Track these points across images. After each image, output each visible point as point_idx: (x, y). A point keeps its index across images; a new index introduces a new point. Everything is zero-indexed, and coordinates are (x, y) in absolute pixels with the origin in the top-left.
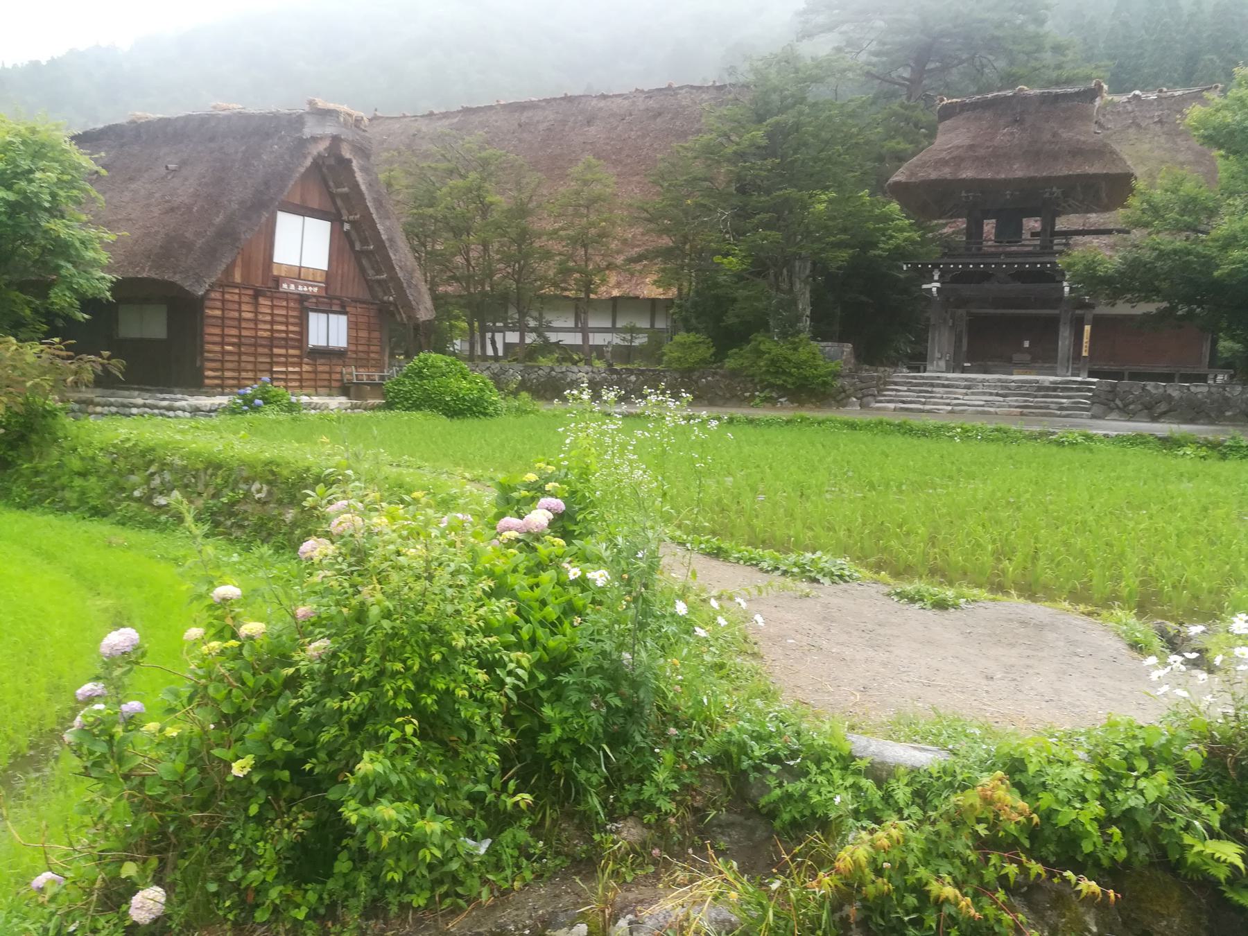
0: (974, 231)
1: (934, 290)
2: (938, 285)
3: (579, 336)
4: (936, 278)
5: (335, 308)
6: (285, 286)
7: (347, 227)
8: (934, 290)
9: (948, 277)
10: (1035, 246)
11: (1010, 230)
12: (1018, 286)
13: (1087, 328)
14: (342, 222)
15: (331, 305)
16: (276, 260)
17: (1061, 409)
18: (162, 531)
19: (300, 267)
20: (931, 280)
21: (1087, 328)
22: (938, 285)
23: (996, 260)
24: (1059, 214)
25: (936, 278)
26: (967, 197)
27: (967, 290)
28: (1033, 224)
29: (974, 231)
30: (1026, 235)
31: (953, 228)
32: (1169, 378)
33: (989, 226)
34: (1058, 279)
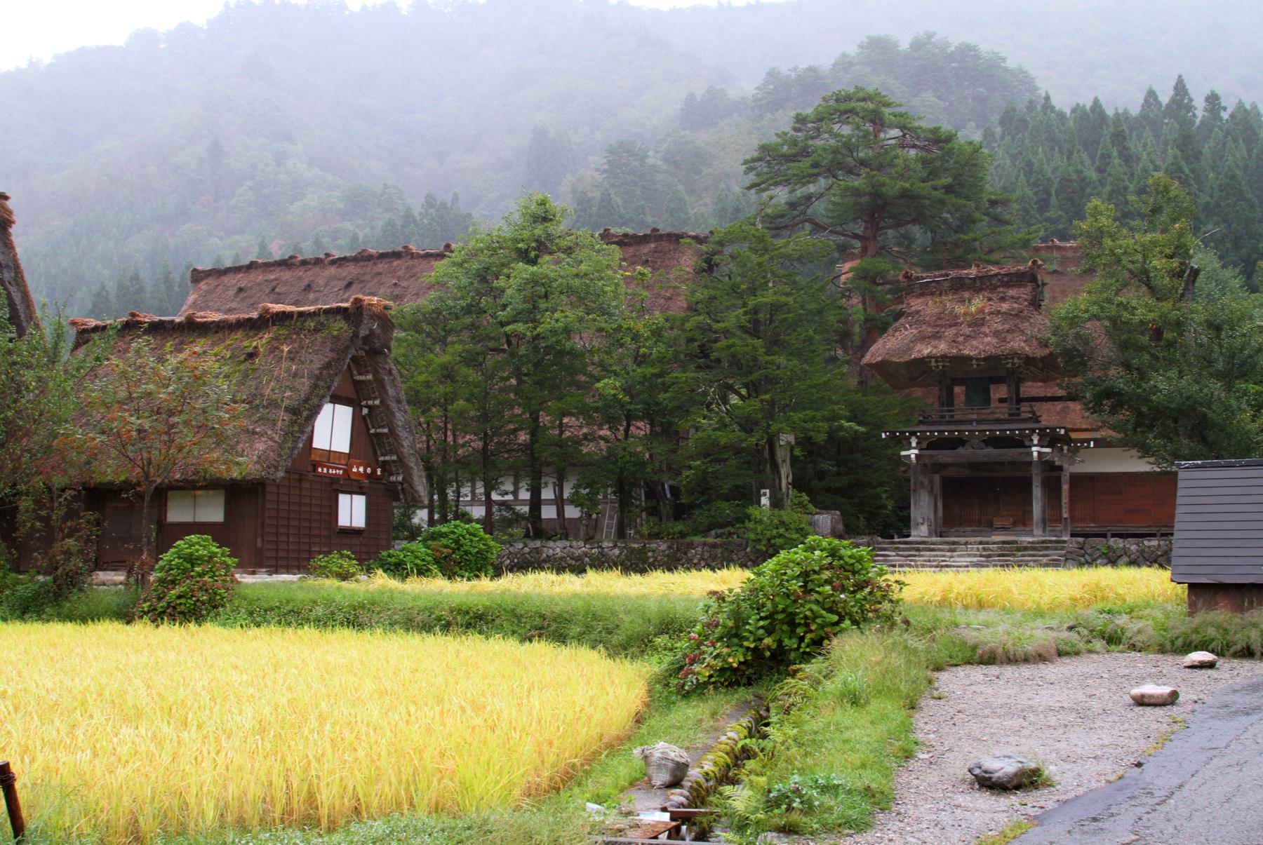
2: (916, 451)
4: (914, 445)
7: (365, 411)
9: (924, 445)
12: (990, 450)
14: (361, 407)
16: (315, 445)
20: (910, 448)
22: (916, 451)
23: (970, 427)
25: (914, 445)
27: (944, 456)
28: (999, 392)
34: (1027, 443)
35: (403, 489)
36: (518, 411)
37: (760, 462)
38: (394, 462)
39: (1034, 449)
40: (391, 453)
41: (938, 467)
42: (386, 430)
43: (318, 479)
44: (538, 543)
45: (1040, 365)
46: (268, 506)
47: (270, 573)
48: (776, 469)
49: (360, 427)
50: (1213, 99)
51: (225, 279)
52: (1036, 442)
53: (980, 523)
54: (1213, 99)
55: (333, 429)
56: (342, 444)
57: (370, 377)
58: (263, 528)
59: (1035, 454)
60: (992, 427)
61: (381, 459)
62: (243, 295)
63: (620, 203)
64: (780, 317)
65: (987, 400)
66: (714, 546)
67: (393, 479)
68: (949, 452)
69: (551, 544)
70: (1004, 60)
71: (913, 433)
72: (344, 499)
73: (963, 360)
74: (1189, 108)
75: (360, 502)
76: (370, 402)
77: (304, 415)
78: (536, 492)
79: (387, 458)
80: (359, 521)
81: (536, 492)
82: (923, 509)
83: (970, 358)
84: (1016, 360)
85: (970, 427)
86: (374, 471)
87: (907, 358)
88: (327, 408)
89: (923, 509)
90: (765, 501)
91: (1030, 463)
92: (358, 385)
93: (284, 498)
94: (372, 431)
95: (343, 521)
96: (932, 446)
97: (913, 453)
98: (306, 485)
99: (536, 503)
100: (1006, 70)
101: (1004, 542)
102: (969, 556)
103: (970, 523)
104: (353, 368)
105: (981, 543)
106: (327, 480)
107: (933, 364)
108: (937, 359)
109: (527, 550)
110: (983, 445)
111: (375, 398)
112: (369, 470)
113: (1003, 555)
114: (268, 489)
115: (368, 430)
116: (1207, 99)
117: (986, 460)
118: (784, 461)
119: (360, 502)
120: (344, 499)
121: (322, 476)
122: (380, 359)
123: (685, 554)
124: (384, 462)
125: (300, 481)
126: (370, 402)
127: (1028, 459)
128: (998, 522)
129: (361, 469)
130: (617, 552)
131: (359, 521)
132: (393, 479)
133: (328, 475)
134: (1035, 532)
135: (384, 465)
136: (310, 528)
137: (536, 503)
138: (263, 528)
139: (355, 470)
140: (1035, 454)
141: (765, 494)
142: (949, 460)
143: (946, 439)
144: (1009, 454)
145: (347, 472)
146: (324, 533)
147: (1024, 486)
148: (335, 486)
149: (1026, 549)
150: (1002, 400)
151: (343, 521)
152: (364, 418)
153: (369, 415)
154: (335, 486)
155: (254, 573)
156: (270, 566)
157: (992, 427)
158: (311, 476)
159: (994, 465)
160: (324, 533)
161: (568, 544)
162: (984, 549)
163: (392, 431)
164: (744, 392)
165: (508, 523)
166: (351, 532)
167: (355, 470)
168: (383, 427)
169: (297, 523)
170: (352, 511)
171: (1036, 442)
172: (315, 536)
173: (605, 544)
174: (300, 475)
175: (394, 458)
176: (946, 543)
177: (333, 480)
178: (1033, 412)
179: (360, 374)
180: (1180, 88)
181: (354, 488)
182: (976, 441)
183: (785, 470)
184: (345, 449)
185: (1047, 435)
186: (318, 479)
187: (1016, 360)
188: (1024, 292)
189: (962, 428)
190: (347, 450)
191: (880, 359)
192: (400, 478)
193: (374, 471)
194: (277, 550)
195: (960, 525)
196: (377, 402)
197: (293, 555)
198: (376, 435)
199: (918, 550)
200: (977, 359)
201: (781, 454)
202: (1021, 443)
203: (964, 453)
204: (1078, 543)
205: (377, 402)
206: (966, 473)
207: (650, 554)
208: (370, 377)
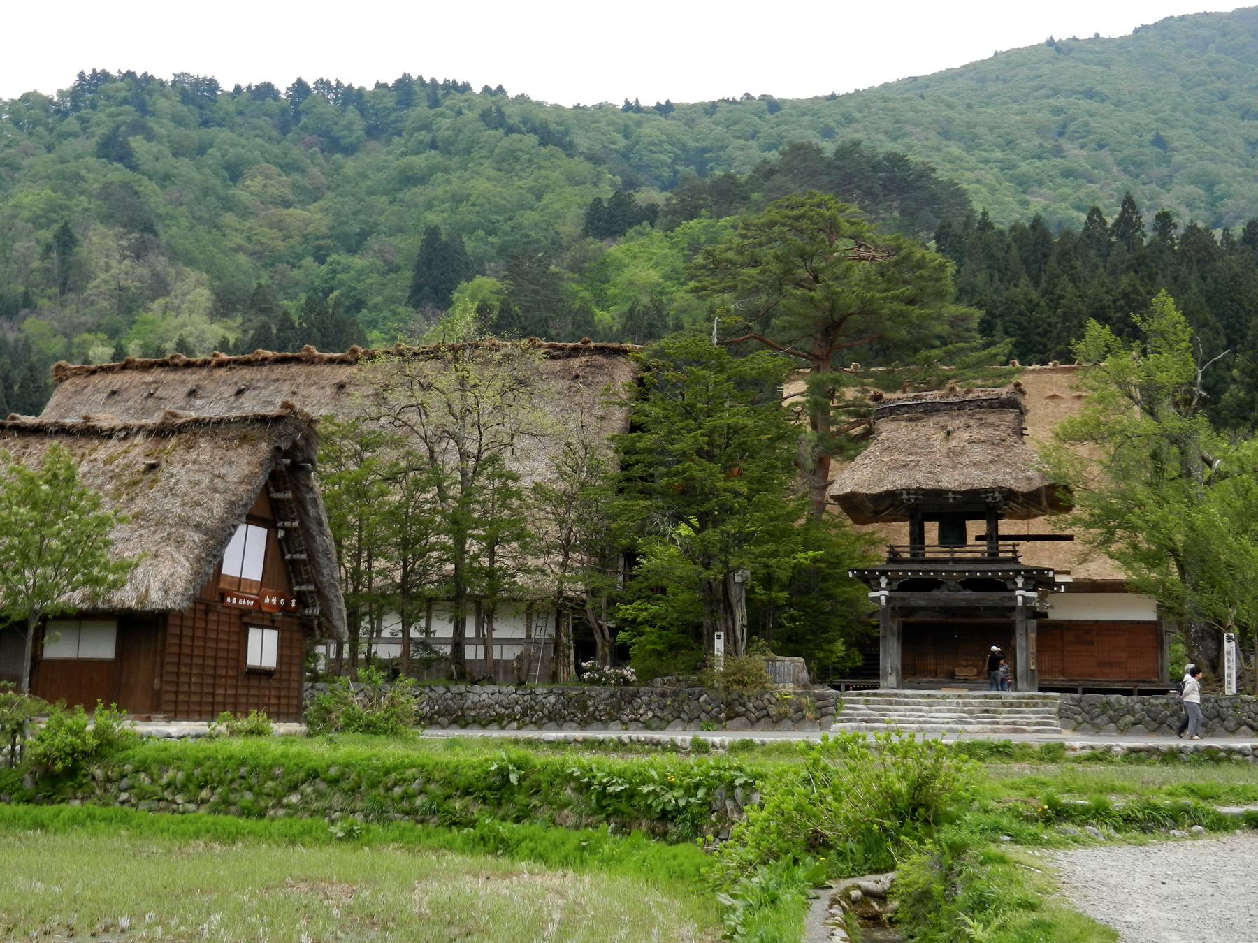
0: (917, 537)
1: (883, 598)
2: (886, 593)
3: (481, 649)
4: (884, 585)
5: (267, 623)
6: (229, 600)
7: (281, 534)
8: (883, 598)
9: (895, 585)
10: (983, 553)
11: (953, 534)
12: (968, 594)
13: (1230, 647)
14: (277, 529)
15: (263, 619)
16: (224, 572)
17: (1028, 724)
18: (37, 804)
19: (240, 579)
20: (878, 588)
21: (1230, 647)
22: (886, 593)
23: (946, 567)
24: (1001, 517)
25: (884, 585)
26: (909, 500)
27: (917, 599)
28: (975, 528)
29: (917, 537)
30: (971, 540)
31: (900, 533)
32: (1128, 693)
33: (932, 531)
34: (1010, 586)
35: (320, 625)
36: (444, 538)
37: (717, 599)
38: (311, 592)
39: (1018, 593)
40: (309, 582)
41: (908, 611)
42: (304, 556)
43: (227, 611)
44: (463, 688)
45: (1021, 499)
46: (170, 640)
47: (169, 720)
48: (729, 609)
49: (276, 552)
50: (1164, 220)
51: (96, 379)
52: (1020, 585)
53: (935, 674)
54: (1164, 220)
55: (246, 556)
56: (254, 572)
57: (289, 495)
58: (162, 666)
59: (1020, 599)
60: (971, 567)
61: (296, 588)
62: (117, 398)
63: (520, 313)
64: (736, 440)
65: (962, 540)
66: (663, 695)
67: (308, 611)
68: (922, 595)
69: (477, 688)
70: (934, 170)
71: (883, 573)
72: (254, 634)
73: (939, 493)
74: (1138, 226)
75: (271, 637)
76: (287, 524)
77: (219, 538)
78: (459, 628)
79: (304, 588)
80: (270, 661)
81: (459, 628)
82: (891, 657)
83: (947, 492)
84: (997, 494)
85: (946, 567)
86: (288, 603)
87: (878, 490)
88: (242, 528)
89: (891, 657)
90: (719, 644)
91: (1014, 608)
92: (275, 505)
93: (187, 632)
94: (288, 557)
95: (253, 660)
96: (904, 587)
97: (883, 594)
98: (213, 617)
99: (458, 643)
100: (936, 182)
101: (986, 697)
102: (949, 711)
103: (926, 673)
104: (270, 484)
105: (959, 696)
106: (235, 612)
107: (905, 496)
108: (909, 491)
109: (449, 695)
110: (958, 586)
111: (293, 519)
112: (282, 601)
113: (987, 711)
114: (171, 621)
115: (283, 555)
116: (1158, 217)
117: (963, 604)
118: (740, 601)
119: (271, 637)
120: (254, 634)
121: (230, 607)
122: (301, 476)
123: (630, 703)
124: (299, 592)
125: (207, 612)
126: (287, 524)
127: (1011, 604)
128: (961, 673)
129: (274, 600)
130: (552, 699)
131: (270, 661)
132: (308, 611)
133: (237, 607)
134: (1019, 686)
135: (300, 597)
136: (215, 668)
137: (458, 643)
138: (162, 666)
139: (267, 601)
140: (1020, 599)
141: (719, 637)
142: (922, 603)
143: (920, 580)
144: (991, 598)
145: (258, 603)
146: (231, 673)
147: (1006, 634)
148: (245, 619)
149: (1012, 705)
150: (978, 538)
151: (253, 660)
152: (280, 541)
153: (286, 538)
154: (245, 619)
155: (148, 719)
156: (166, 712)
157: (971, 567)
158: (219, 607)
159: (970, 611)
160: (231, 673)
161: (496, 689)
162: (965, 704)
163: (311, 557)
164: (694, 521)
165: (427, 664)
166: (261, 674)
167: (267, 601)
168: (301, 552)
169: (200, 662)
170: (263, 648)
171: (1020, 585)
172: (221, 677)
173: (539, 691)
174: (207, 605)
175: (312, 588)
176: (923, 696)
177: (244, 612)
178: (1015, 552)
179: (278, 491)
180: (1129, 204)
181: (267, 622)
182: (953, 583)
183: (740, 612)
184: (257, 577)
185: (1033, 578)
186: (227, 611)
187: (997, 494)
188: (1011, 415)
189: (939, 567)
190: (259, 578)
191: (849, 490)
192: (317, 612)
193: (288, 603)
194: (176, 693)
195: (914, 675)
196: (296, 524)
197: (195, 698)
198: (292, 561)
199: (890, 703)
200: (954, 492)
201: (734, 592)
202: (1001, 586)
203: (940, 595)
204: (1072, 699)
205: (296, 524)
206: (940, 618)
207: (590, 703)
208: (289, 495)
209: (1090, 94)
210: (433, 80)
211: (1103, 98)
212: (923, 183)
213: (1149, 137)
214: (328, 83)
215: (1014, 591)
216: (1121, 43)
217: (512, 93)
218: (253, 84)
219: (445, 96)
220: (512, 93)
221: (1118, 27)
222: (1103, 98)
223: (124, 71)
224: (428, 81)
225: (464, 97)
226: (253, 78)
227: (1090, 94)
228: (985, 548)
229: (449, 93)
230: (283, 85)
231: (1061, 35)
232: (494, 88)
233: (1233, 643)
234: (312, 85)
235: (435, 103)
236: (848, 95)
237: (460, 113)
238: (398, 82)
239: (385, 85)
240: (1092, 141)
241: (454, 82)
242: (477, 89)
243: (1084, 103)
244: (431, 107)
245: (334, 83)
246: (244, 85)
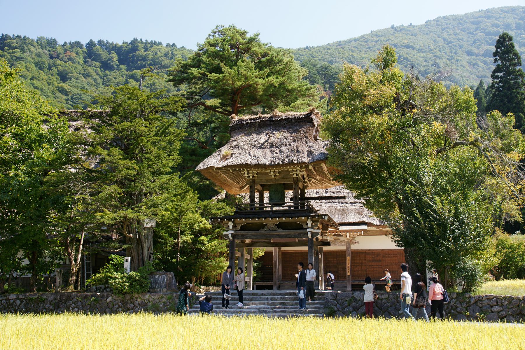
2: (232, 232)
4: (231, 227)
20: (228, 229)
25: (231, 227)
34: (305, 226)
52: (310, 225)
171: (310, 225)
209: (408, 47)
210: (146, 41)
211: (413, 48)
212: (337, 76)
213: (431, 63)
214: (103, 41)
215: (306, 229)
216: (421, 28)
217: (179, 46)
218: (72, 42)
219: (151, 47)
220: (179, 46)
221: (419, 21)
222: (413, 48)
223: (16, 35)
224: (144, 41)
225: (158, 47)
226: (71, 39)
227: (408, 47)
228: (292, 204)
229: (152, 46)
230: (84, 42)
231: (397, 24)
232: (171, 44)
233: (135, 276)
234: (96, 43)
235: (146, 50)
236: (313, 47)
237: (156, 54)
238: (132, 41)
239: (127, 43)
240: (409, 64)
241: (155, 41)
242: (164, 45)
243: (406, 50)
244: (145, 51)
245: (105, 42)
246: (68, 42)
